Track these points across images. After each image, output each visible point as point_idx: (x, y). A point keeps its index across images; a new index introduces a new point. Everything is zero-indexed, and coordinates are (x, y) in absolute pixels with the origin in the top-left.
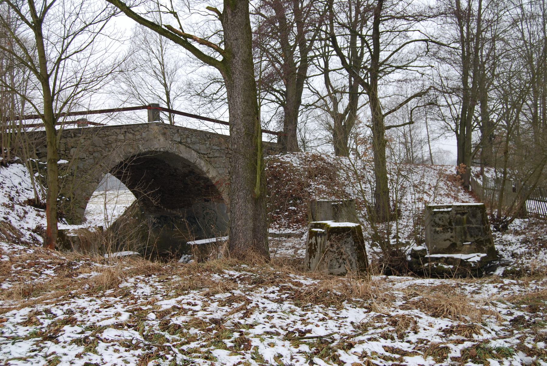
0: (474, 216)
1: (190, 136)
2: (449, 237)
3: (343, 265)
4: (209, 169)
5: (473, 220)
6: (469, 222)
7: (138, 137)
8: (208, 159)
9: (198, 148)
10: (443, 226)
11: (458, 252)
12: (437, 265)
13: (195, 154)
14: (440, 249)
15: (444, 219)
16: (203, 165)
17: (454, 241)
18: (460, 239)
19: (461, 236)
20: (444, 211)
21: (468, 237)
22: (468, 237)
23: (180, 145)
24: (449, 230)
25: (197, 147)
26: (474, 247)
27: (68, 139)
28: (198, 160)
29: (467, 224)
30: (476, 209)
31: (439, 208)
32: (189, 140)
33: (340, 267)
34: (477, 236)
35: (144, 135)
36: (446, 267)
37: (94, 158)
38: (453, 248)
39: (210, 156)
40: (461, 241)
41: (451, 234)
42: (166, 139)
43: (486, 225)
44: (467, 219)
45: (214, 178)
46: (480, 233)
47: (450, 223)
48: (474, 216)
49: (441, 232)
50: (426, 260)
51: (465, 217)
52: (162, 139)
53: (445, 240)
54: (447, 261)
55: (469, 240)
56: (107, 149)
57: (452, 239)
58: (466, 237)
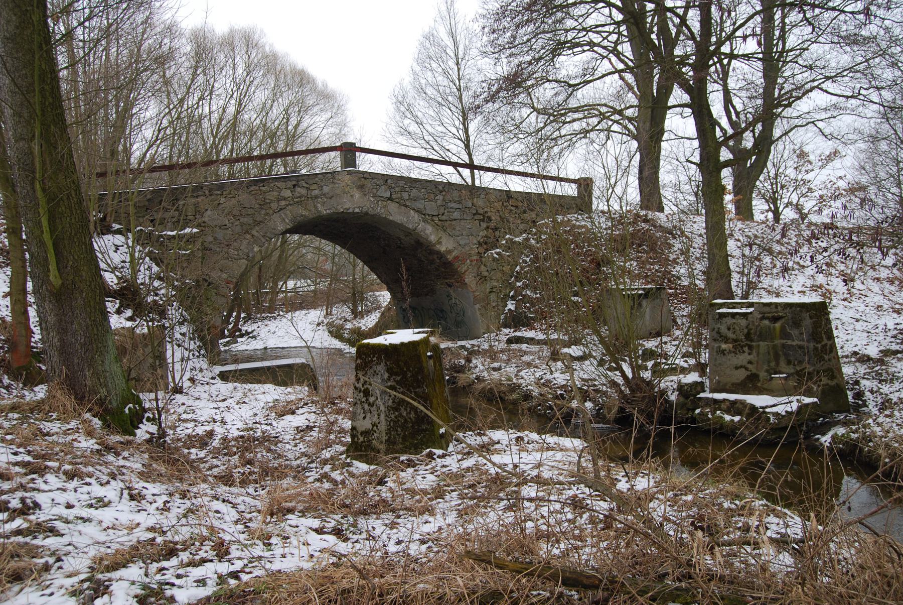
0: (797, 324)
1: (407, 189)
2: (745, 363)
3: (369, 415)
4: (441, 238)
5: (794, 332)
6: (785, 335)
7: (316, 192)
8: (439, 223)
9: (421, 207)
10: (735, 341)
11: (760, 391)
12: (713, 413)
13: (416, 215)
14: (726, 384)
15: (737, 328)
16: (430, 233)
17: (754, 371)
18: (765, 367)
19: (769, 362)
20: (737, 314)
21: (783, 364)
22: (783, 364)
23: (389, 202)
24: (746, 349)
25: (419, 205)
26: (792, 383)
27: (199, 199)
28: (422, 225)
29: (781, 338)
30: (801, 311)
31: (734, 308)
32: (405, 195)
33: (364, 418)
34: (800, 362)
35: (326, 189)
36: (728, 418)
37: (242, 224)
38: (751, 384)
39: (444, 218)
40: (767, 371)
41: (749, 357)
42: (365, 195)
43: (825, 341)
44: (783, 328)
45: (450, 252)
46: (806, 358)
47: (748, 336)
48: (797, 324)
49: (730, 352)
50: (698, 403)
51: (778, 325)
52: (357, 194)
53: (737, 368)
54: (733, 407)
55: (783, 370)
56: (263, 212)
57: (749, 366)
58: (778, 364)
